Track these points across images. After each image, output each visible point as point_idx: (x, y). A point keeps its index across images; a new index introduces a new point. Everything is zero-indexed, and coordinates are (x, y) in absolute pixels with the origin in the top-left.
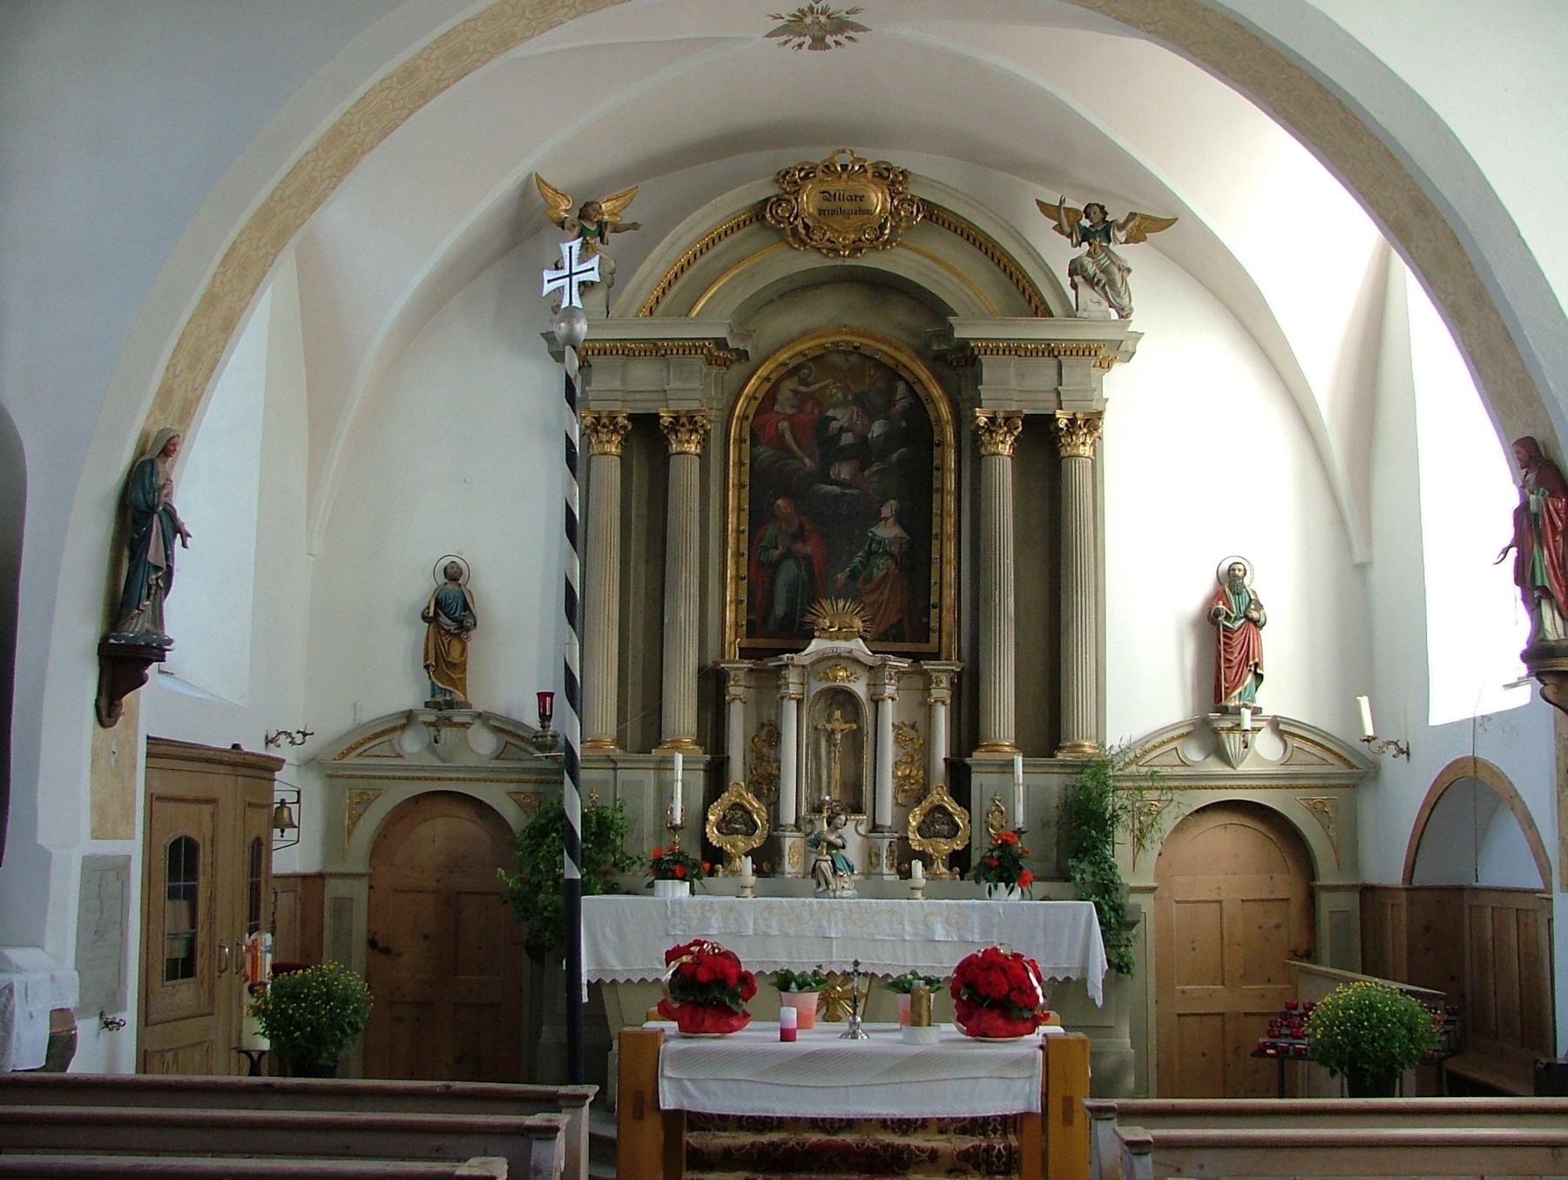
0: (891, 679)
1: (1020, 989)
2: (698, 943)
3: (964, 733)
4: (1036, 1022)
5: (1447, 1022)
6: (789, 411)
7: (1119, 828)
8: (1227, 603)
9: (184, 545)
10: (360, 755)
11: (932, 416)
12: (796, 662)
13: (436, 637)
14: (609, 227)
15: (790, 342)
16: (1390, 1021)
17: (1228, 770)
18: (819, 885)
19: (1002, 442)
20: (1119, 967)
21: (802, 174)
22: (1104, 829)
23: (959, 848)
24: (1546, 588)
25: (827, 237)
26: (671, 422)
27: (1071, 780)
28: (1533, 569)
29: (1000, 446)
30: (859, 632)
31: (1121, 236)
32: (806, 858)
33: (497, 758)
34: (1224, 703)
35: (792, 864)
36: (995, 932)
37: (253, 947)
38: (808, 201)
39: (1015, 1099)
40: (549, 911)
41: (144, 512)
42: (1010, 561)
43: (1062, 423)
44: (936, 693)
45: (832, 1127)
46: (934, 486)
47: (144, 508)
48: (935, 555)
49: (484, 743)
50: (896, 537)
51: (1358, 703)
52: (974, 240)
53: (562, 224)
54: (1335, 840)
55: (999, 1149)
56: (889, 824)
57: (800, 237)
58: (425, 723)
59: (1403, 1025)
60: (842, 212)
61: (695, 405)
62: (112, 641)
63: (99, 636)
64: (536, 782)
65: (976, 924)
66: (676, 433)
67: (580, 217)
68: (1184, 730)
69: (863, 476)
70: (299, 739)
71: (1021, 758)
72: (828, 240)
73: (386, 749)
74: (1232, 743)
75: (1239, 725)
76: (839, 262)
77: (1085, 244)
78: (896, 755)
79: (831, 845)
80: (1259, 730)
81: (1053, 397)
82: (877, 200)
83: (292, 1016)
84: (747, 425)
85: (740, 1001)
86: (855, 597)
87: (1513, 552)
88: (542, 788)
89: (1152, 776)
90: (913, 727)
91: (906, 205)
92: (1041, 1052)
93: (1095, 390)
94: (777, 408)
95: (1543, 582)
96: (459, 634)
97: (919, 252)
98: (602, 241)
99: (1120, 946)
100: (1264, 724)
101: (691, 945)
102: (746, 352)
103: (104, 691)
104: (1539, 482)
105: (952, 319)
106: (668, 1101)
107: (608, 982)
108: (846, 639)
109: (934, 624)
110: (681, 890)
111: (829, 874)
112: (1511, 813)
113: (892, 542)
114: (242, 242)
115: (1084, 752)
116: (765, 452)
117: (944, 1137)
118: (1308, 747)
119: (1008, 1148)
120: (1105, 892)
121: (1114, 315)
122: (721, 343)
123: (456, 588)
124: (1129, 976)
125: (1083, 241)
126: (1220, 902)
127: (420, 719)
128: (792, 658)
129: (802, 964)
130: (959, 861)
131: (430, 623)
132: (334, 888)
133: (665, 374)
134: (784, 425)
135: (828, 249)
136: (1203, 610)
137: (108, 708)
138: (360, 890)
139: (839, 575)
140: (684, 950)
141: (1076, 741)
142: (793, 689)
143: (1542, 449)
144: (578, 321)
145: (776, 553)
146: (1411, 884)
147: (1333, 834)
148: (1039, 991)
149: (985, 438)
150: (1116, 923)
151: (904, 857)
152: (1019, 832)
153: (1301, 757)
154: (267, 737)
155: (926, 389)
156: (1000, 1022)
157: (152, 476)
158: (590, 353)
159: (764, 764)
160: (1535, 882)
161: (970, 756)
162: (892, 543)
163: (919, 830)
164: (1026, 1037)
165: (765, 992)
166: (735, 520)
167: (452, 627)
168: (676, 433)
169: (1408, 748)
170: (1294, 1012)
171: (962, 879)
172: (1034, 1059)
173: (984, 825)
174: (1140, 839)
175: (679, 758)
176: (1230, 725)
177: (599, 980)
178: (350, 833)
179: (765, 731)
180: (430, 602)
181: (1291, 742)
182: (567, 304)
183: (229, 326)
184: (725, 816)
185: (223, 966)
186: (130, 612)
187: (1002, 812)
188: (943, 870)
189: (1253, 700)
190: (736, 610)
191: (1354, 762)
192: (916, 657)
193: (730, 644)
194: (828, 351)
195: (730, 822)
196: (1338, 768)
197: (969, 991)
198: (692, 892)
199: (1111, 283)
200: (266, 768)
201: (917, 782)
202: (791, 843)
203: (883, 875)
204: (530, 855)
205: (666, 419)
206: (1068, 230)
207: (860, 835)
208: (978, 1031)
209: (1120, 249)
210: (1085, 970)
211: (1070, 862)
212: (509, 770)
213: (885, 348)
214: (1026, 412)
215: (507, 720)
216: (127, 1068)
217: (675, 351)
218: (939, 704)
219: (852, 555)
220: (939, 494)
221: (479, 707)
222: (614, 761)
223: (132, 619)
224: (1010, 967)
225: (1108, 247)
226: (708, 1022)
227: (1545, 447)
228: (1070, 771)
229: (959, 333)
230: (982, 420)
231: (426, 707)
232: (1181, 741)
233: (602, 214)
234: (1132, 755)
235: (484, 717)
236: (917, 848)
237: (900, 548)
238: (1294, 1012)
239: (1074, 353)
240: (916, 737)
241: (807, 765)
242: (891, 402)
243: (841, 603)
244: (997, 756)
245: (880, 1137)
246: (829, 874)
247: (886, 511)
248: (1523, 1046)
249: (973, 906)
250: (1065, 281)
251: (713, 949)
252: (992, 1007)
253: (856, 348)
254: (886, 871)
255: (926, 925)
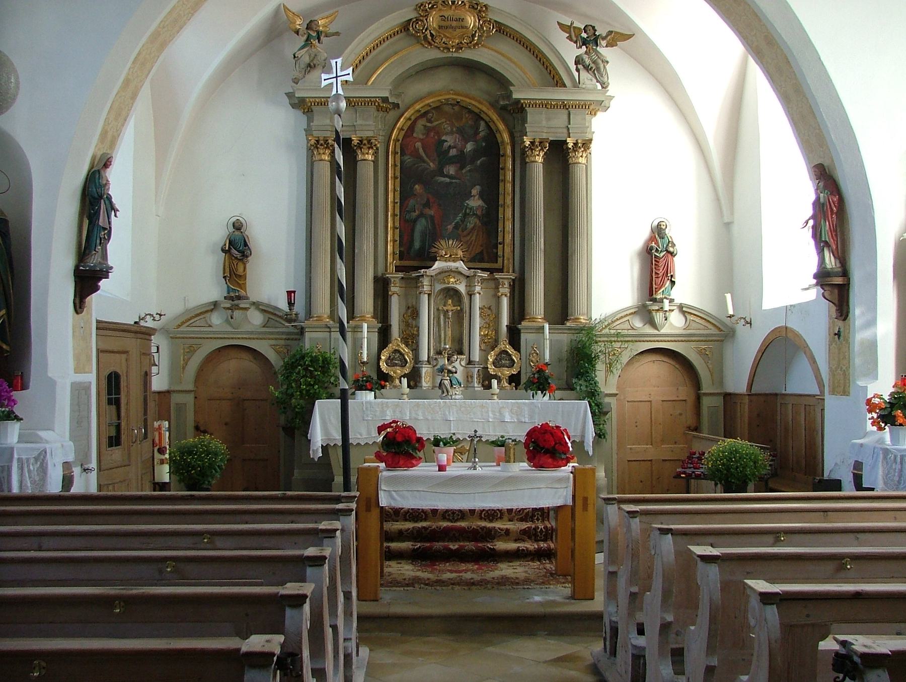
0: (478, 283)
1: (560, 443)
2: (394, 422)
3: (516, 311)
4: (568, 461)
5: (772, 460)
6: (421, 137)
7: (599, 363)
8: (657, 243)
9: (115, 216)
10: (188, 326)
11: (499, 140)
12: (428, 274)
13: (229, 262)
14: (323, 35)
15: (421, 99)
16: (745, 458)
17: (656, 332)
18: (443, 392)
19: (538, 155)
20: (600, 435)
21: (430, 6)
22: (592, 363)
23: (515, 373)
24: (827, 242)
25: (443, 41)
26: (358, 143)
27: (574, 337)
28: (821, 231)
29: (537, 157)
30: (460, 257)
31: (604, 43)
32: (434, 378)
33: (264, 327)
34: (654, 296)
35: (426, 383)
36: (537, 416)
37: (160, 428)
38: (433, 21)
39: (559, 498)
40: (299, 409)
41: (96, 199)
42: (542, 220)
43: (570, 145)
44: (502, 290)
45: (453, 519)
46: (500, 178)
47: (96, 196)
48: (501, 216)
49: (256, 319)
50: (479, 206)
51: (725, 297)
52: (523, 44)
53: (297, 32)
54: (711, 369)
55: (541, 529)
56: (478, 360)
57: (428, 41)
58: (224, 308)
59: (751, 460)
60: (452, 27)
61: (370, 134)
62: (81, 268)
63: (74, 265)
64: (285, 339)
65: (526, 413)
66: (361, 149)
67: (307, 28)
68: (633, 311)
69: (462, 173)
70: (157, 317)
71: (548, 325)
72: (444, 43)
73: (202, 323)
74: (659, 317)
75: (662, 308)
76: (450, 55)
77: (584, 47)
78: (480, 323)
79: (450, 372)
80: (673, 310)
81: (565, 131)
82: (471, 21)
83: (190, 463)
84: (398, 144)
85: (417, 451)
86: (458, 238)
87: (811, 223)
88: (289, 342)
89: (618, 335)
90: (489, 308)
91: (487, 24)
92: (572, 475)
93: (588, 127)
94: (415, 135)
95: (825, 238)
96: (242, 259)
97: (492, 50)
98: (319, 41)
99: (600, 424)
100: (675, 307)
101: (391, 423)
102: (398, 104)
103: (78, 296)
104: (825, 187)
105: (512, 88)
106: (384, 501)
107: (332, 445)
108: (454, 261)
109: (500, 253)
110: (369, 396)
111: (449, 387)
112: (804, 355)
113: (478, 209)
114: (143, 50)
115: (581, 322)
116: (408, 159)
117: (511, 523)
118: (698, 320)
119: (546, 527)
120: (592, 395)
121: (599, 87)
122: (385, 100)
123: (240, 234)
124: (605, 440)
125: (583, 45)
126: (650, 401)
127: (222, 306)
128: (426, 272)
129: (443, 433)
130: (514, 380)
131: (226, 253)
132: (176, 399)
133: (354, 116)
134: (418, 145)
135: (443, 48)
136: (643, 248)
137: (79, 305)
138: (189, 399)
139: (449, 227)
140: (389, 425)
141: (576, 316)
142: (426, 288)
143: (827, 170)
144: (342, 101)
145: (414, 215)
146: (751, 392)
147: (710, 366)
148: (570, 445)
149: (529, 153)
150: (599, 412)
151: (486, 380)
152: (547, 364)
153: (694, 325)
154: (139, 317)
155: (495, 125)
156: (550, 460)
157: (99, 179)
158: (313, 104)
159: (410, 328)
160: (815, 390)
161: (521, 324)
162: (477, 209)
163: (494, 363)
164: (563, 468)
165: (429, 447)
166: (392, 196)
167: (239, 255)
168: (361, 149)
169: (751, 321)
170: (694, 456)
171: (516, 389)
172: (569, 478)
173: (528, 361)
174: (610, 367)
175: (365, 325)
176: (657, 308)
177: (328, 444)
178: (184, 368)
179: (410, 311)
180: (226, 241)
181: (689, 317)
182: (335, 93)
183: (134, 97)
184: (390, 357)
185: (134, 440)
186: (91, 252)
187: (537, 354)
188: (507, 385)
189: (669, 295)
190: (393, 245)
191: (722, 328)
192: (491, 271)
193: (390, 264)
194: (442, 104)
195: (393, 359)
196: (714, 331)
197: (534, 445)
198: (375, 398)
199: (598, 69)
200: (148, 333)
201: (492, 338)
202: (425, 370)
203: (474, 387)
204: (287, 379)
205: (355, 141)
206: (575, 39)
207: (463, 366)
208: (539, 466)
209: (603, 51)
210: (583, 436)
211: (574, 381)
212: (272, 333)
213: (474, 103)
214: (551, 139)
215: (269, 306)
216: (93, 489)
217: (360, 104)
218: (504, 296)
219: (456, 215)
220: (503, 183)
221: (253, 298)
222: (329, 327)
223: (92, 256)
224: (555, 432)
225: (596, 49)
226: (401, 462)
227: (828, 169)
228: (573, 332)
229: (516, 96)
230: (527, 143)
231: (225, 299)
232: (631, 316)
233: (319, 26)
234: (606, 323)
235: (257, 305)
236: (493, 373)
237: (482, 212)
238: (694, 456)
239: (577, 107)
240: (491, 314)
241: (433, 330)
242: (477, 133)
243: (451, 242)
244: (534, 324)
245: (479, 524)
246: (449, 387)
247: (475, 191)
248: (806, 475)
249: (524, 404)
250: (573, 67)
251: (403, 424)
252: (546, 452)
253: (458, 102)
254: (476, 385)
255: (501, 414)
